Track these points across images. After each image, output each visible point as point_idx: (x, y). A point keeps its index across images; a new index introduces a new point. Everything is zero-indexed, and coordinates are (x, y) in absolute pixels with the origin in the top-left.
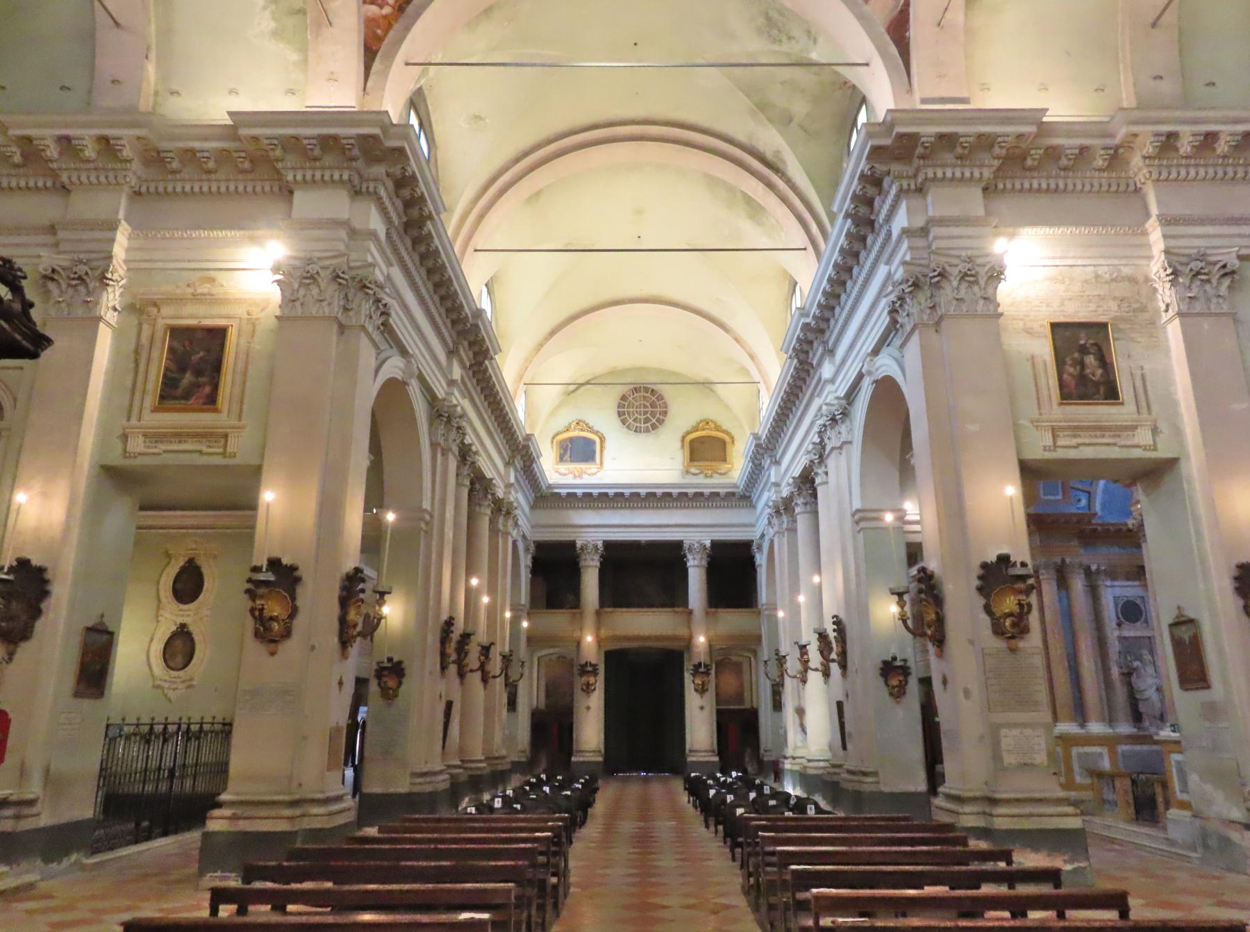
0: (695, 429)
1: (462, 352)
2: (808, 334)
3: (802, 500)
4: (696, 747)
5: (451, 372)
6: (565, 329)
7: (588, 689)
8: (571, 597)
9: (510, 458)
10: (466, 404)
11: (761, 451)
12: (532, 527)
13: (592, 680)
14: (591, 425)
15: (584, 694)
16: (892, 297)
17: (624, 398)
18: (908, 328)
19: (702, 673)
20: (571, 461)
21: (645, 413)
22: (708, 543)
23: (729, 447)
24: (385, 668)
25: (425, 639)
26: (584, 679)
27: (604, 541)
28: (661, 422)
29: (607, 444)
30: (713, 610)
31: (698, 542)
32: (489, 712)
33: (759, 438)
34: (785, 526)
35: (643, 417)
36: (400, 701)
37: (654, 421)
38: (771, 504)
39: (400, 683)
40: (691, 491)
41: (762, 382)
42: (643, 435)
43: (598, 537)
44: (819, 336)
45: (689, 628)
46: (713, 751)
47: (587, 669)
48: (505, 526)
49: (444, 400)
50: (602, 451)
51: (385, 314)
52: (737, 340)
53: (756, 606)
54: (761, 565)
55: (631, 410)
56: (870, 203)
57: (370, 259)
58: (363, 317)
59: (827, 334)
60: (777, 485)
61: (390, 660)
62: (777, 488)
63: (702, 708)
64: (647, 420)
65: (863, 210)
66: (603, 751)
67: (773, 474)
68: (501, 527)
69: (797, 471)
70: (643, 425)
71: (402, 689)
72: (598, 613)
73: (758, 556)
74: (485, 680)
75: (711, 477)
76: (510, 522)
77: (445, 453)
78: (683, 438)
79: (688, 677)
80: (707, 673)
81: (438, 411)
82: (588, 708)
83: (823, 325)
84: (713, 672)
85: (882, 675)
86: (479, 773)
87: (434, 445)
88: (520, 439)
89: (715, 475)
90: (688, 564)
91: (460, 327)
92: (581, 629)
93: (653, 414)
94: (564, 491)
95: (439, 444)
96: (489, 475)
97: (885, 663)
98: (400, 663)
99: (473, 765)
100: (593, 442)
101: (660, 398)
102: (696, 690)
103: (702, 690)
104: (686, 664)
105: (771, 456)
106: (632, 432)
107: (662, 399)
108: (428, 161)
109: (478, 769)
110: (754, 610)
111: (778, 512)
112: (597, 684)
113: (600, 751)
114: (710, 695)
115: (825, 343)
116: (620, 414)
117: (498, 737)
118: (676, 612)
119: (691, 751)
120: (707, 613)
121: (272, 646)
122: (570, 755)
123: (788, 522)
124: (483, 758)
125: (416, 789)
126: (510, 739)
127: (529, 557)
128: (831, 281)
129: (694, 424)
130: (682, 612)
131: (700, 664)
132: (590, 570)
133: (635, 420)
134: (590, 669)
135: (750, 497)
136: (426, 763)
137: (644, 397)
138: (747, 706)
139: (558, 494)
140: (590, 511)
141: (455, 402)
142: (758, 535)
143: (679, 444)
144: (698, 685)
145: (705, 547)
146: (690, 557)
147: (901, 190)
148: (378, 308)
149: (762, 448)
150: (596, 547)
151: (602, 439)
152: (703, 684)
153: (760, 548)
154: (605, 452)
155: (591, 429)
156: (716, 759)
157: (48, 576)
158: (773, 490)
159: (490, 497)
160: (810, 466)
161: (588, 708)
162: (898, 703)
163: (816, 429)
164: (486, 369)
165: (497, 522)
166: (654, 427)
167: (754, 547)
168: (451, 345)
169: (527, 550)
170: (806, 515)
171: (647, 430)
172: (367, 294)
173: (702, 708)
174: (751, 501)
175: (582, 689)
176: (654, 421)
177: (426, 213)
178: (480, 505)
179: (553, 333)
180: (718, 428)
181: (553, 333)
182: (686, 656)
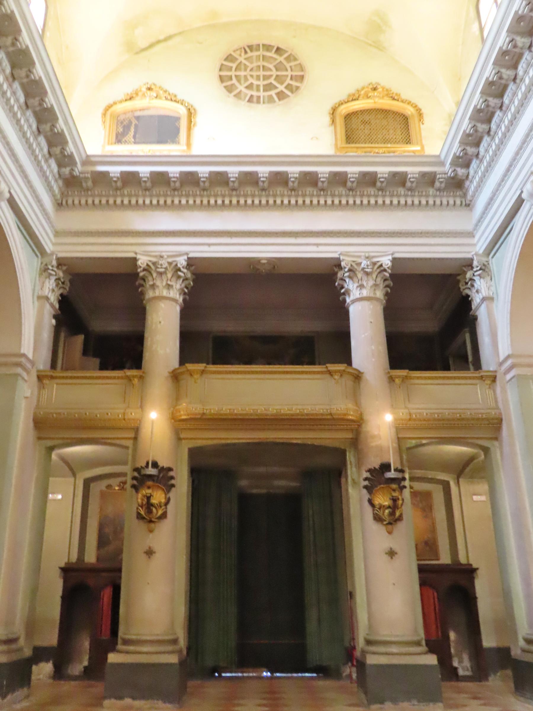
0: (353, 98)
13: (158, 497)
15: (142, 526)
20: (135, 143)
23: (413, 124)
29: (199, 119)
35: (261, 83)
42: (261, 108)
45: (357, 402)
46: (418, 644)
50: (189, 129)
55: (242, 73)
63: (391, 553)
64: (269, 87)
66: (183, 643)
78: (334, 110)
82: (150, 553)
92: (142, 407)
94: (115, 170)
102: (378, 519)
108: (42, 37)
113: (175, 641)
116: (222, 79)
118: (330, 373)
119: (369, 642)
120: (391, 379)
121: (390, 527)
129: (352, 90)
130: (342, 373)
132: (162, 305)
133: (250, 87)
137: (264, 56)
139: (105, 174)
143: (327, 119)
145: (381, 269)
146: (351, 285)
147: (447, 174)
151: (191, 113)
155: (173, 99)
168: (59, 197)
171: (270, 100)
173: (391, 553)
175: (139, 517)
182: (350, 457)
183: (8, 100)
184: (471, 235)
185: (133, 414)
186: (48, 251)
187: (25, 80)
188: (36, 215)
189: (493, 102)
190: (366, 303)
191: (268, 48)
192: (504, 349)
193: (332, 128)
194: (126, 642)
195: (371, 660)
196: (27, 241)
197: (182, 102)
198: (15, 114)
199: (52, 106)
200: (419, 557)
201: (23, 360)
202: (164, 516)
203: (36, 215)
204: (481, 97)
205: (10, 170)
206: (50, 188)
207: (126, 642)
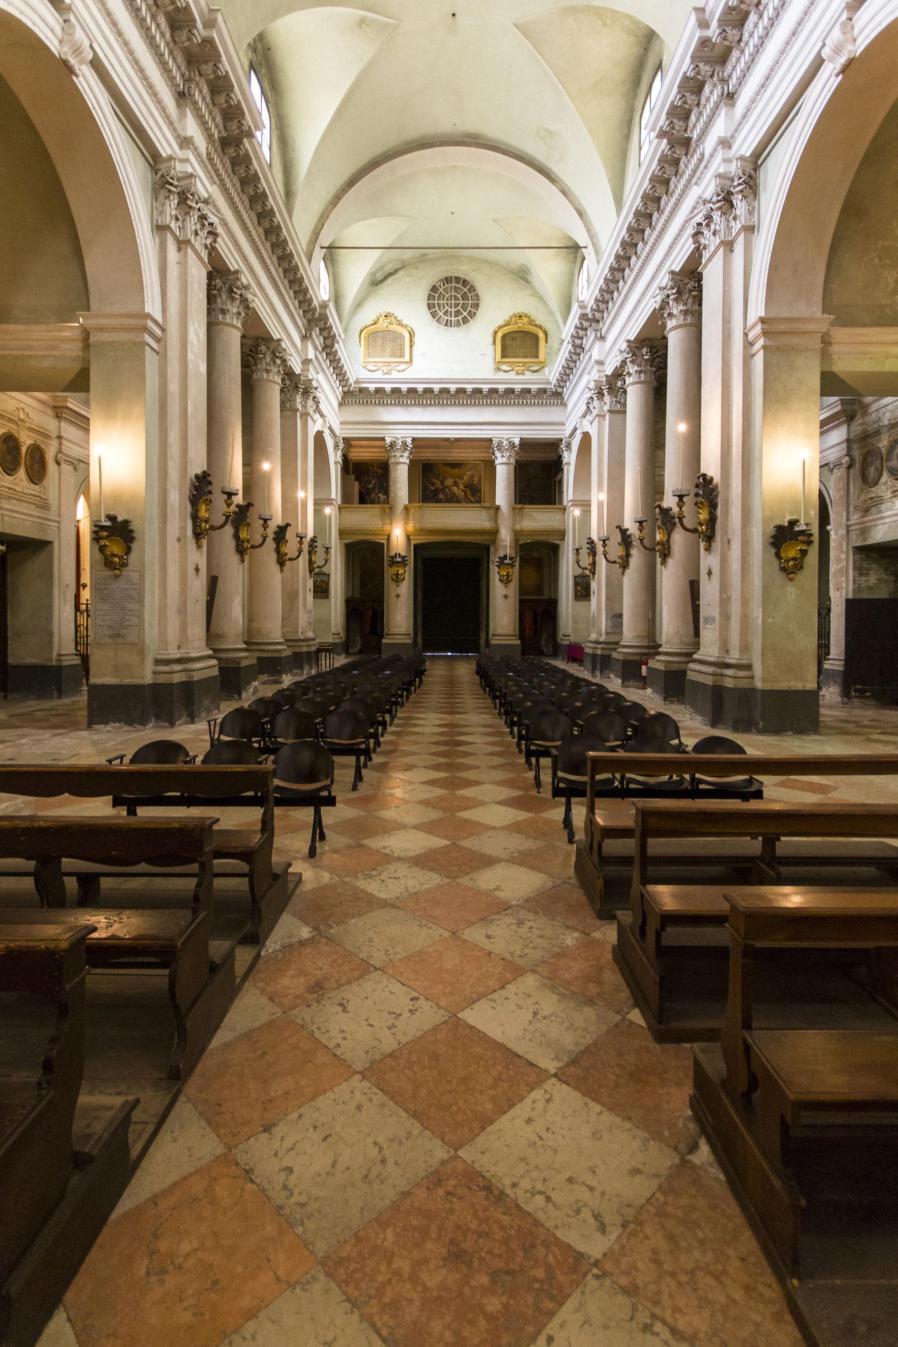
1: (314, 336)
2: (584, 322)
3: (681, 307)
4: (500, 631)
5: (184, 128)
6: (365, 180)
7: (397, 579)
9: (342, 398)
10: (321, 377)
11: (585, 324)
12: (341, 423)
14: (399, 318)
16: (699, 219)
17: (434, 289)
18: (712, 248)
19: (508, 564)
21: (456, 305)
22: (517, 441)
24: (103, 528)
25: (164, 494)
26: (394, 570)
27: (414, 440)
28: (472, 315)
30: (520, 506)
31: (507, 440)
33: (585, 307)
36: (130, 573)
37: (465, 314)
38: (592, 385)
39: (128, 550)
40: (501, 387)
41: (590, 247)
42: (453, 329)
43: (407, 434)
44: (594, 325)
46: (515, 636)
47: (398, 561)
48: (304, 406)
49: (300, 375)
51: (213, 234)
52: (564, 192)
53: (561, 502)
54: (568, 464)
55: (441, 302)
56: (686, 117)
57: (190, 170)
59: (601, 324)
60: (600, 363)
61: (112, 518)
62: (601, 368)
63: (506, 597)
64: (458, 313)
65: (678, 124)
67: (596, 352)
68: (299, 407)
70: (453, 319)
71: (133, 557)
73: (565, 454)
75: (523, 374)
77: (182, 244)
79: (494, 571)
80: (512, 565)
81: (163, 176)
82: (398, 596)
83: (598, 315)
84: (517, 564)
85: (773, 544)
86: (276, 655)
87: (160, 229)
89: (528, 373)
90: (497, 462)
91: (309, 316)
93: (464, 307)
95: (168, 228)
96: (233, 265)
97: (779, 528)
98: (126, 523)
100: (402, 337)
101: (472, 289)
102: (501, 581)
103: (505, 581)
105: (596, 330)
106: (442, 327)
107: (475, 290)
109: (279, 651)
110: (557, 506)
111: (600, 394)
112: (406, 575)
113: (409, 634)
114: (514, 585)
115: (724, 81)
116: (430, 307)
119: (494, 635)
122: (382, 637)
123: (611, 403)
124: (282, 640)
125: (162, 679)
127: (339, 453)
129: (507, 318)
131: (505, 557)
132: (400, 467)
133: (446, 313)
134: (399, 559)
135: (560, 394)
137: (455, 288)
138: (546, 596)
139: (367, 389)
140: (399, 408)
142: (568, 433)
144: (504, 576)
145: (512, 445)
148: (203, 225)
149: (588, 320)
150: (404, 444)
151: (412, 335)
152: (508, 575)
153: (569, 446)
156: (518, 642)
158: (596, 368)
159: (278, 361)
161: (398, 596)
162: (791, 580)
163: (690, 231)
165: (295, 401)
166: (465, 321)
167: (563, 446)
169: (336, 446)
170: (639, 386)
171: (458, 324)
172: (170, 191)
173: (506, 597)
174: (563, 399)
175: (392, 579)
176: (465, 314)
179: (352, 182)
180: (532, 322)
181: (352, 182)
182: (492, 549)
183: (149, 29)
184: (563, 424)
186: (164, 155)
187: (171, 8)
189: (691, 98)
190: (505, 466)
191: (457, 279)
192: (571, 497)
193: (493, 347)
194: (388, 635)
195: (493, 642)
196: (134, 140)
197: (406, 326)
199: (227, 72)
200: (520, 595)
201: (150, 324)
202: (404, 579)
204: (667, 119)
205: (98, 25)
206: (171, 79)
207: (388, 635)
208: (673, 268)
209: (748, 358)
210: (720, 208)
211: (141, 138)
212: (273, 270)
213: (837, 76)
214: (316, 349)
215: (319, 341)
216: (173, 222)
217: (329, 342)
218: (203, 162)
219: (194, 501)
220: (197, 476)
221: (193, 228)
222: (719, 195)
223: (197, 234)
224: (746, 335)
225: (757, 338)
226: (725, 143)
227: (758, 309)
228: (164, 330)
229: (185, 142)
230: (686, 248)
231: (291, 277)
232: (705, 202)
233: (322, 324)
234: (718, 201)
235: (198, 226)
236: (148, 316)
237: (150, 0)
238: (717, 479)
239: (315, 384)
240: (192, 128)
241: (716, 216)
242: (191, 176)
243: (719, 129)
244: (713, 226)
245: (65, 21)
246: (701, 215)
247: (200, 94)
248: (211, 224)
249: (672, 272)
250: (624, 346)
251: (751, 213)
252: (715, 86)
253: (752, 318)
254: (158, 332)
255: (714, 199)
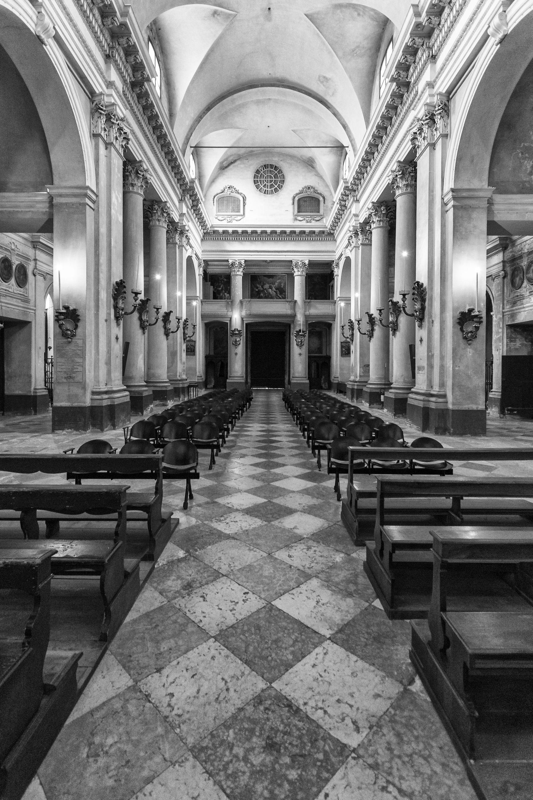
3: (404, 183)
6: (216, 107)
7: (236, 344)
8: (227, 295)
10: (190, 224)
11: (347, 192)
12: (203, 251)
14: (237, 189)
17: (258, 172)
18: (423, 147)
21: (271, 181)
22: (307, 262)
24: (61, 314)
26: (234, 339)
27: (245, 261)
28: (280, 187)
32: (172, 355)
33: (347, 183)
34: (360, 242)
36: (78, 340)
39: (76, 327)
41: (350, 147)
43: (241, 258)
44: (352, 193)
48: (180, 241)
51: (127, 139)
52: (335, 114)
53: (333, 298)
56: (407, 69)
57: (113, 101)
58: (112, 138)
59: (357, 192)
60: (356, 215)
61: (66, 308)
62: (357, 218)
63: (300, 354)
64: (272, 186)
65: (403, 74)
67: (354, 209)
68: (178, 241)
69: (402, 156)
72: (241, 302)
73: (336, 270)
74: (167, 334)
75: (310, 222)
76: (184, 239)
77: (108, 145)
78: (294, 198)
81: (96, 104)
82: (236, 354)
83: (355, 187)
84: (307, 335)
86: (164, 389)
88: (187, 179)
90: (295, 274)
93: (276, 182)
95: (99, 135)
96: (138, 158)
98: (75, 310)
99: (158, 385)
101: (280, 171)
102: (297, 345)
103: (300, 345)
104: (292, 330)
105: (354, 196)
109: (166, 387)
110: (331, 301)
111: (356, 234)
115: (430, 48)
116: (255, 182)
117: (180, 368)
122: (227, 378)
123: (363, 239)
126: (190, 370)
127: (201, 269)
128: (374, 136)
129: (301, 189)
131: (300, 331)
132: (237, 277)
133: (264, 186)
134: (237, 332)
135: (333, 234)
136: (106, 384)
138: (324, 354)
139: (218, 231)
141: (184, 224)
142: (337, 257)
145: (304, 264)
148: (121, 134)
149: (349, 190)
150: (240, 263)
151: (244, 199)
153: (337, 265)
154: (246, 206)
157: (78, 313)
158: (354, 218)
159: (165, 215)
160: (369, 218)
163: (410, 137)
164: (200, 209)
165: (175, 238)
166: (276, 190)
167: (334, 265)
169: (200, 265)
171: (272, 192)
173: (300, 354)
177: (146, 76)
178: (159, 220)
180: (315, 191)
181: (209, 108)
182: (292, 326)
183: (88, 17)
185: (229, 313)
188: (80, 51)
189: (410, 58)
196: (79, 83)
198: (85, 12)
199: (135, 43)
201: (89, 192)
203: (80, 51)
204: (411, 37)
208: (399, 159)
209: (444, 213)
210: (428, 123)
211: (84, 82)
212: (162, 160)
213: (497, 45)
214: (188, 207)
215: (189, 203)
216: (103, 132)
217: (195, 203)
218: (120, 96)
219: (115, 298)
220: (117, 283)
221: (115, 135)
222: (427, 116)
223: (117, 139)
224: (443, 199)
225: (449, 201)
226: (431, 85)
227: (450, 184)
228: (97, 196)
229: (110, 84)
230: (407, 147)
231: (173, 165)
232: (418, 120)
233: (191, 193)
234: (426, 120)
235: (118, 134)
236: (88, 188)
237: (89, 0)
238: (425, 285)
239: (187, 228)
240: (114, 76)
241: (425, 128)
242: (113, 104)
243: (427, 77)
244: (423, 134)
245: (39, 13)
246: (416, 128)
247: (119, 56)
248: (125, 133)
249: (399, 162)
250: (370, 205)
251: (446, 127)
252: (424, 51)
253: (447, 189)
254: (94, 197)
255: (424, 119)
